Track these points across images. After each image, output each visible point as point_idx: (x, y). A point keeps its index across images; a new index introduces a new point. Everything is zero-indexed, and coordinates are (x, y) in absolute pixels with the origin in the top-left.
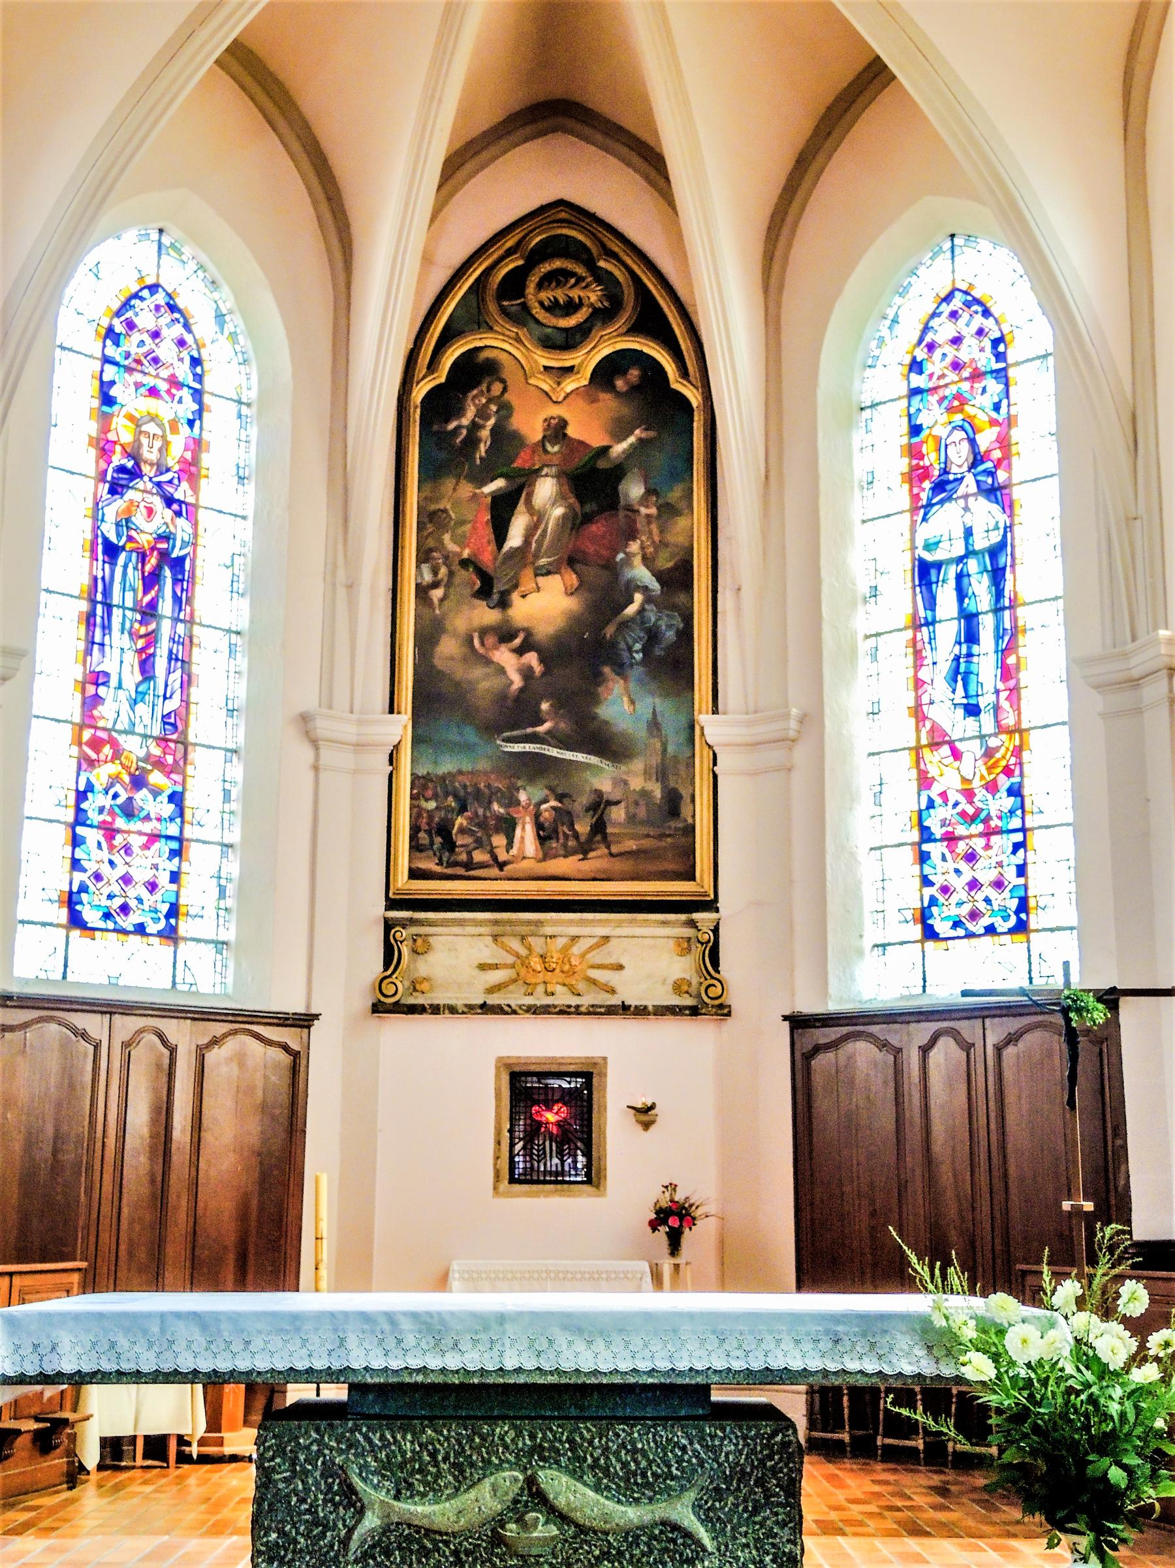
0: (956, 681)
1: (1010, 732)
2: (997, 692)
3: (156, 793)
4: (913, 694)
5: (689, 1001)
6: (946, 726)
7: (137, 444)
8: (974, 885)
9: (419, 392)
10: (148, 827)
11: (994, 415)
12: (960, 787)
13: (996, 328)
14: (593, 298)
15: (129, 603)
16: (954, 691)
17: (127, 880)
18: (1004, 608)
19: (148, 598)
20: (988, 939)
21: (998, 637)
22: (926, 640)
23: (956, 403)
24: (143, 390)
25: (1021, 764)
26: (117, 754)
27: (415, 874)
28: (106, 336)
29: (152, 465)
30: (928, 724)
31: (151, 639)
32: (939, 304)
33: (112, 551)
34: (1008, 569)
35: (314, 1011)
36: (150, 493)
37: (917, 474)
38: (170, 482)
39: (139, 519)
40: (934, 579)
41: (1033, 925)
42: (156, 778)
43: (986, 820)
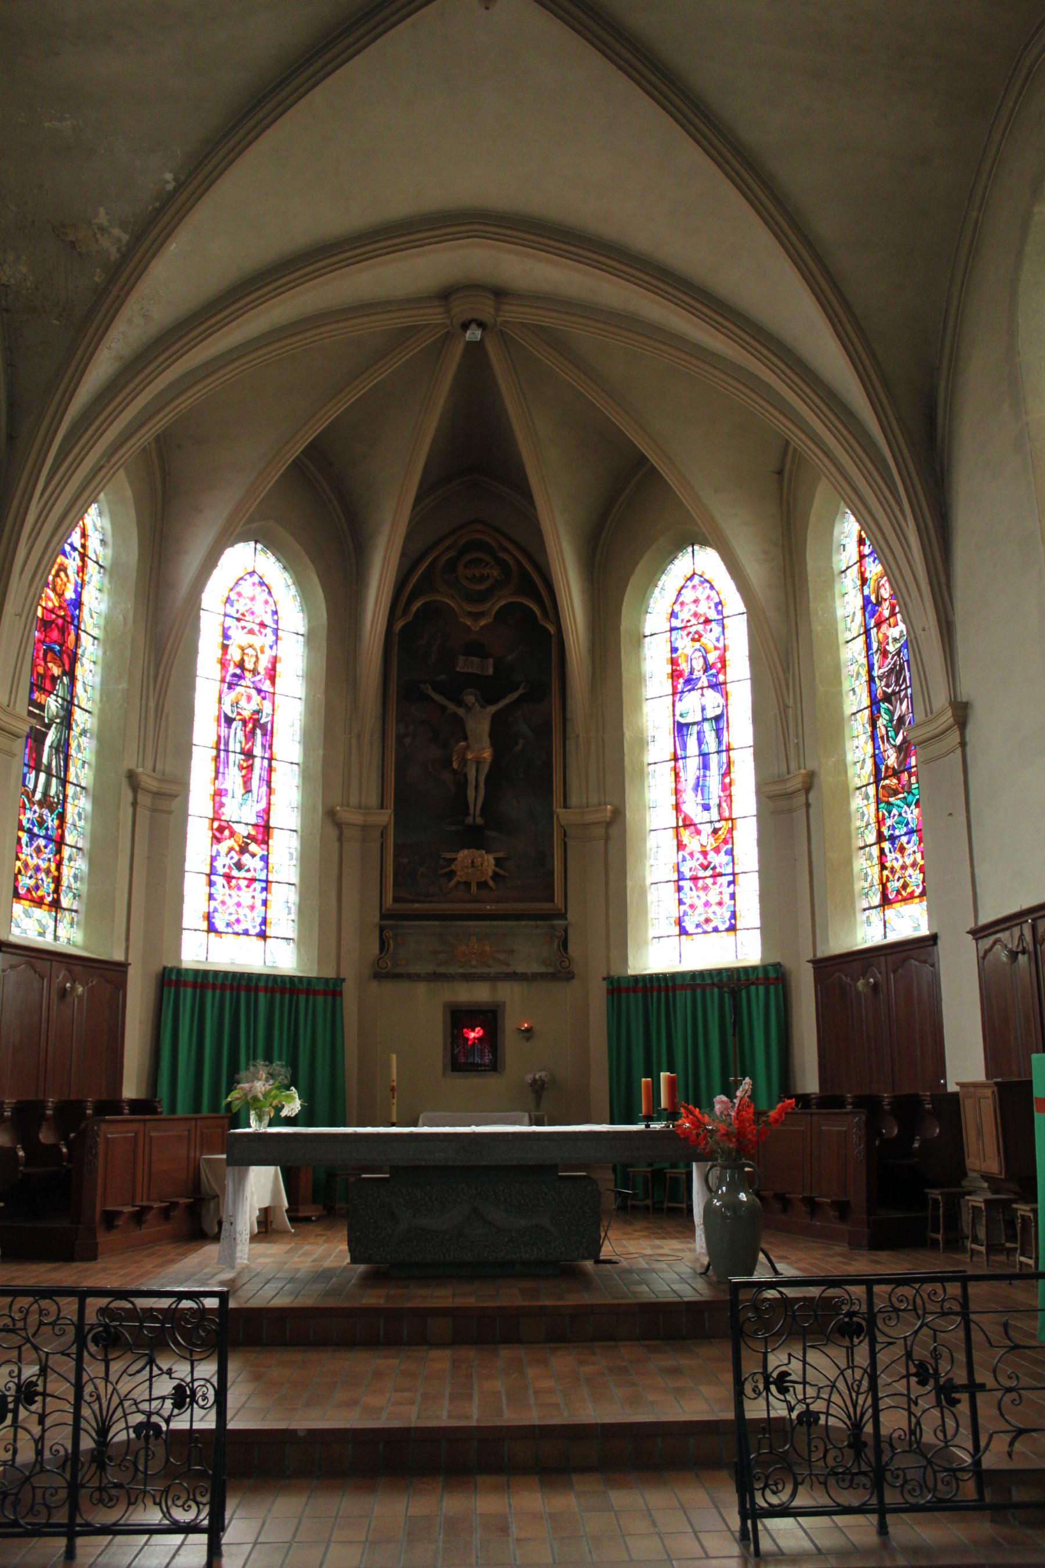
0: (697, 791)
1: (726, 820)
2: (720, 797)
3: (253, 855)
4: (674, 797)
5: (551, 970)
6: (692, 816)
7: (242, 660)
8: (707, 904)
9: (399, 625)
10: (249, 875)
11: (717, 644)
12: (700, 850)
13: (716, 596)
14: (495, 574)
15: (238, 750)
16: (696, 796)
17: (239, 905)
18: (722, 751)
19: (247, 747)
20: (714, 934)
21: (720, 767)
22: (681, 767)
23: (696, 636)
24: (246, 630)
25: (732, 838)
26: (232, 834)
27: (396, 900)
28: (226, 602)
29: (250, 671)
30: (683, 815)
31: (250, 768)
32: (686, 581)
33: (229, 721)
34: (725, 729)
35: (342, 977)
36: (249, 687)
37: (675, 675)
38: (260, 681)
39: (243, 703)
40: (685, 733)
41: (738, 927)
42: (253, 847)
43: (714, 868)
